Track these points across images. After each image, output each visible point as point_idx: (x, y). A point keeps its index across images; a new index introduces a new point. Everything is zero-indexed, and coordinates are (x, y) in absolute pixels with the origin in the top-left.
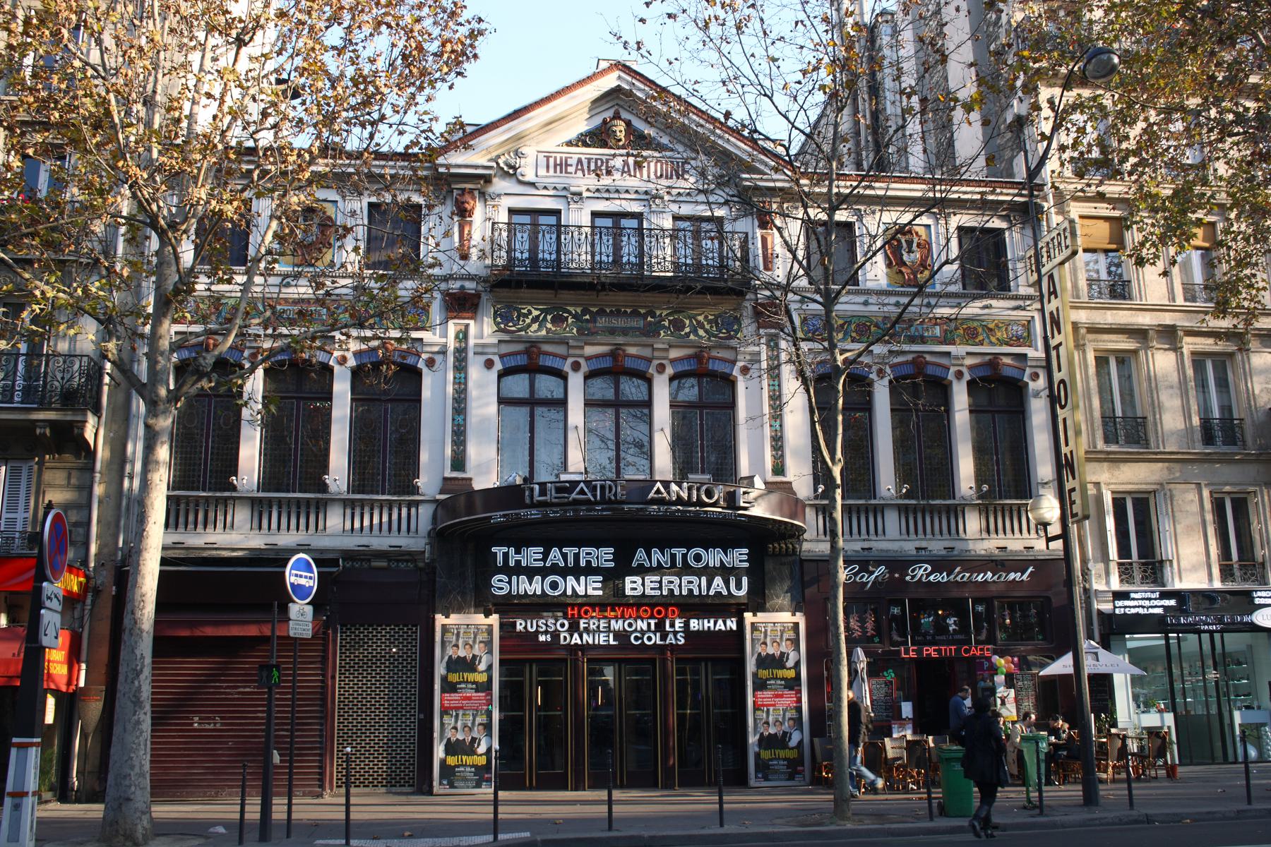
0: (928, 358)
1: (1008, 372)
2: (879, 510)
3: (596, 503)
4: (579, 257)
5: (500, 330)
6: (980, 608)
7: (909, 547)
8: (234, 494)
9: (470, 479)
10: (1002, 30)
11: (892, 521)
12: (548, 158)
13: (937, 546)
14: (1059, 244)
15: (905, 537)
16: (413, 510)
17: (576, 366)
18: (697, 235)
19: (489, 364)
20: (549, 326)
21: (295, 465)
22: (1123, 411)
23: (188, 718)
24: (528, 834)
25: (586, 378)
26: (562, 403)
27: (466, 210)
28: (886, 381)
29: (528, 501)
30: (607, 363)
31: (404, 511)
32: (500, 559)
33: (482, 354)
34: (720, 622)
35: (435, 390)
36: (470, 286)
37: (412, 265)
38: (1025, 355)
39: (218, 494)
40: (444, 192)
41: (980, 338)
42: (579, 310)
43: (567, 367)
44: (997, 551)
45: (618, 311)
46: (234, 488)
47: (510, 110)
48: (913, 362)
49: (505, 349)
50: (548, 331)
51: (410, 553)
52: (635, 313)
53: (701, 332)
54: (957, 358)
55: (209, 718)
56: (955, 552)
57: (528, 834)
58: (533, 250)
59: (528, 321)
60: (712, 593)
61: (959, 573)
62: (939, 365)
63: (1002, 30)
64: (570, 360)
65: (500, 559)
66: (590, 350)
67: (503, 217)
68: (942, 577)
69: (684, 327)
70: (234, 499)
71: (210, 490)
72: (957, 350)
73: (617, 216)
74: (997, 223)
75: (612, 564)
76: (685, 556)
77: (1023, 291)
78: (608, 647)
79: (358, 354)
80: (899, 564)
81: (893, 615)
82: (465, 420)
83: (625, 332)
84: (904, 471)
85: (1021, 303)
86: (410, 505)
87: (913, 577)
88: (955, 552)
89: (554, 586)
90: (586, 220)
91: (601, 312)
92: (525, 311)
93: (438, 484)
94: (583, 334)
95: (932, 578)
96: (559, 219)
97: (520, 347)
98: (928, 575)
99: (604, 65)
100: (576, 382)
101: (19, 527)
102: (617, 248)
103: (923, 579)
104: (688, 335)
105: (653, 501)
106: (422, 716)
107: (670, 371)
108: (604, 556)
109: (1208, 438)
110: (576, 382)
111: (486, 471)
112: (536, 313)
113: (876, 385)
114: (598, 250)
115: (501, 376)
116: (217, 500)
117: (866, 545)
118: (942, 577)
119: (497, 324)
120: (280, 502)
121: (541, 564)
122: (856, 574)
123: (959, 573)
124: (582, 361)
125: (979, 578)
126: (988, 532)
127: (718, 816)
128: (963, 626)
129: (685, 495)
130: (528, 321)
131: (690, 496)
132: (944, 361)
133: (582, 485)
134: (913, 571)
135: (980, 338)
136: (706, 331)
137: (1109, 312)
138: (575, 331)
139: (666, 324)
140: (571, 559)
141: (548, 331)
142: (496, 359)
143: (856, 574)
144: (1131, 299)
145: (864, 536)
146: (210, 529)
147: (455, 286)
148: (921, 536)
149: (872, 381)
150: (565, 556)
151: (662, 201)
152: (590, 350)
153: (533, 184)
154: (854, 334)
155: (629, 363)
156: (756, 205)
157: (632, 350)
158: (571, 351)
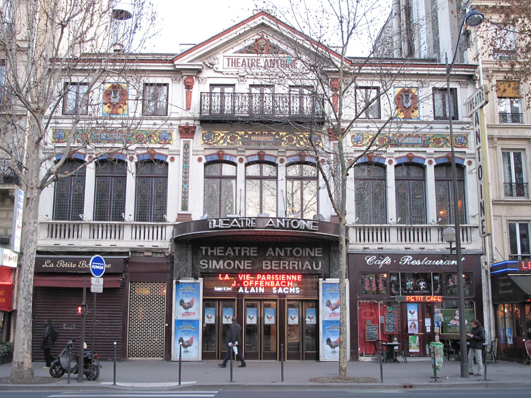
0: (415, 154)
3: (242, 228)
6: (437, 278)
7: (401, 247)
8: (82, 222)
9: (190, 215)
12: (229, 59)
13: (416, 247)
14: (480, 97)
16: (164, 229)
19: (200, 160)
20: (229, 141)
21: (109, 208)
22: (516, 181)
23: (61, 324)
24: (195, 382)
28: (133, 164)
29: (210, 227)
31: (160, 229)
33: (196, 155)
34: (264, 276)
35: (174, 171)
36: (191, 123)
37: (162, 113)
39: (74, 222)
40: (179, 77)
41: (442, 144)
42: (243, 133)
43: (278, 162)
44: (419, 250)
46: (81, 219)
47: (210, 37)
48: (407, 156)
49: (208, 152)
50: (228, 143)
51: (162, 249)
53: (302, 143)
55: (70, 325)
56: (425, 250)
57: (195, 382)
58: (301, 107)
59: (218, 139)
60: (304, 268)
61: (426, 261)
62: (420, 158)
64: (238, 157)
66: (248, 153)
68: (418, 263)
69: (293, 141)
70: (82, 224)
72: (391, 150)
77: (466, 120)
78: (295, 294)
80: (396, 256)
81: (393, 281)
82: (188, 186)
85: (464, 126)
87: (403, 262)
88: (425, 250)
89: (229, 265)
92: (217, 134)
93: (176, 217)
94: (245, 145)
95: (412, 263)
96: (234, 89)
97: (215, 151)
98: (411, 261)
103: (408, 263)
104: (295, 144)
105: (268, 227)
106: (167, 325)
108: (252, 252)
111: (197, 213)
112: (222, 135)
114: (292, 105)
115: (206, 165)
117: (380, 246)
118: (418, 263)
119: (204, 140)
121: (223, 254)
123: (426, 261)
125: (436, 263)
127: (116, 380)
128: (428, 288)
129: (283, 225)
130: (218, 139)
132: (423, 155)
133: (235, 220)
134: (403, 259)
135: (442, 144)
136: (304, 143)
137: (510, 130)
138: (241, 143)
139: (285, 139)
141: (228, 143)
143: (374, 261)
146: (71, 238)
147: (183, 123)
149: (465, 166)
152: (248, 153)
154: (229, 141)
158: (280, 154)
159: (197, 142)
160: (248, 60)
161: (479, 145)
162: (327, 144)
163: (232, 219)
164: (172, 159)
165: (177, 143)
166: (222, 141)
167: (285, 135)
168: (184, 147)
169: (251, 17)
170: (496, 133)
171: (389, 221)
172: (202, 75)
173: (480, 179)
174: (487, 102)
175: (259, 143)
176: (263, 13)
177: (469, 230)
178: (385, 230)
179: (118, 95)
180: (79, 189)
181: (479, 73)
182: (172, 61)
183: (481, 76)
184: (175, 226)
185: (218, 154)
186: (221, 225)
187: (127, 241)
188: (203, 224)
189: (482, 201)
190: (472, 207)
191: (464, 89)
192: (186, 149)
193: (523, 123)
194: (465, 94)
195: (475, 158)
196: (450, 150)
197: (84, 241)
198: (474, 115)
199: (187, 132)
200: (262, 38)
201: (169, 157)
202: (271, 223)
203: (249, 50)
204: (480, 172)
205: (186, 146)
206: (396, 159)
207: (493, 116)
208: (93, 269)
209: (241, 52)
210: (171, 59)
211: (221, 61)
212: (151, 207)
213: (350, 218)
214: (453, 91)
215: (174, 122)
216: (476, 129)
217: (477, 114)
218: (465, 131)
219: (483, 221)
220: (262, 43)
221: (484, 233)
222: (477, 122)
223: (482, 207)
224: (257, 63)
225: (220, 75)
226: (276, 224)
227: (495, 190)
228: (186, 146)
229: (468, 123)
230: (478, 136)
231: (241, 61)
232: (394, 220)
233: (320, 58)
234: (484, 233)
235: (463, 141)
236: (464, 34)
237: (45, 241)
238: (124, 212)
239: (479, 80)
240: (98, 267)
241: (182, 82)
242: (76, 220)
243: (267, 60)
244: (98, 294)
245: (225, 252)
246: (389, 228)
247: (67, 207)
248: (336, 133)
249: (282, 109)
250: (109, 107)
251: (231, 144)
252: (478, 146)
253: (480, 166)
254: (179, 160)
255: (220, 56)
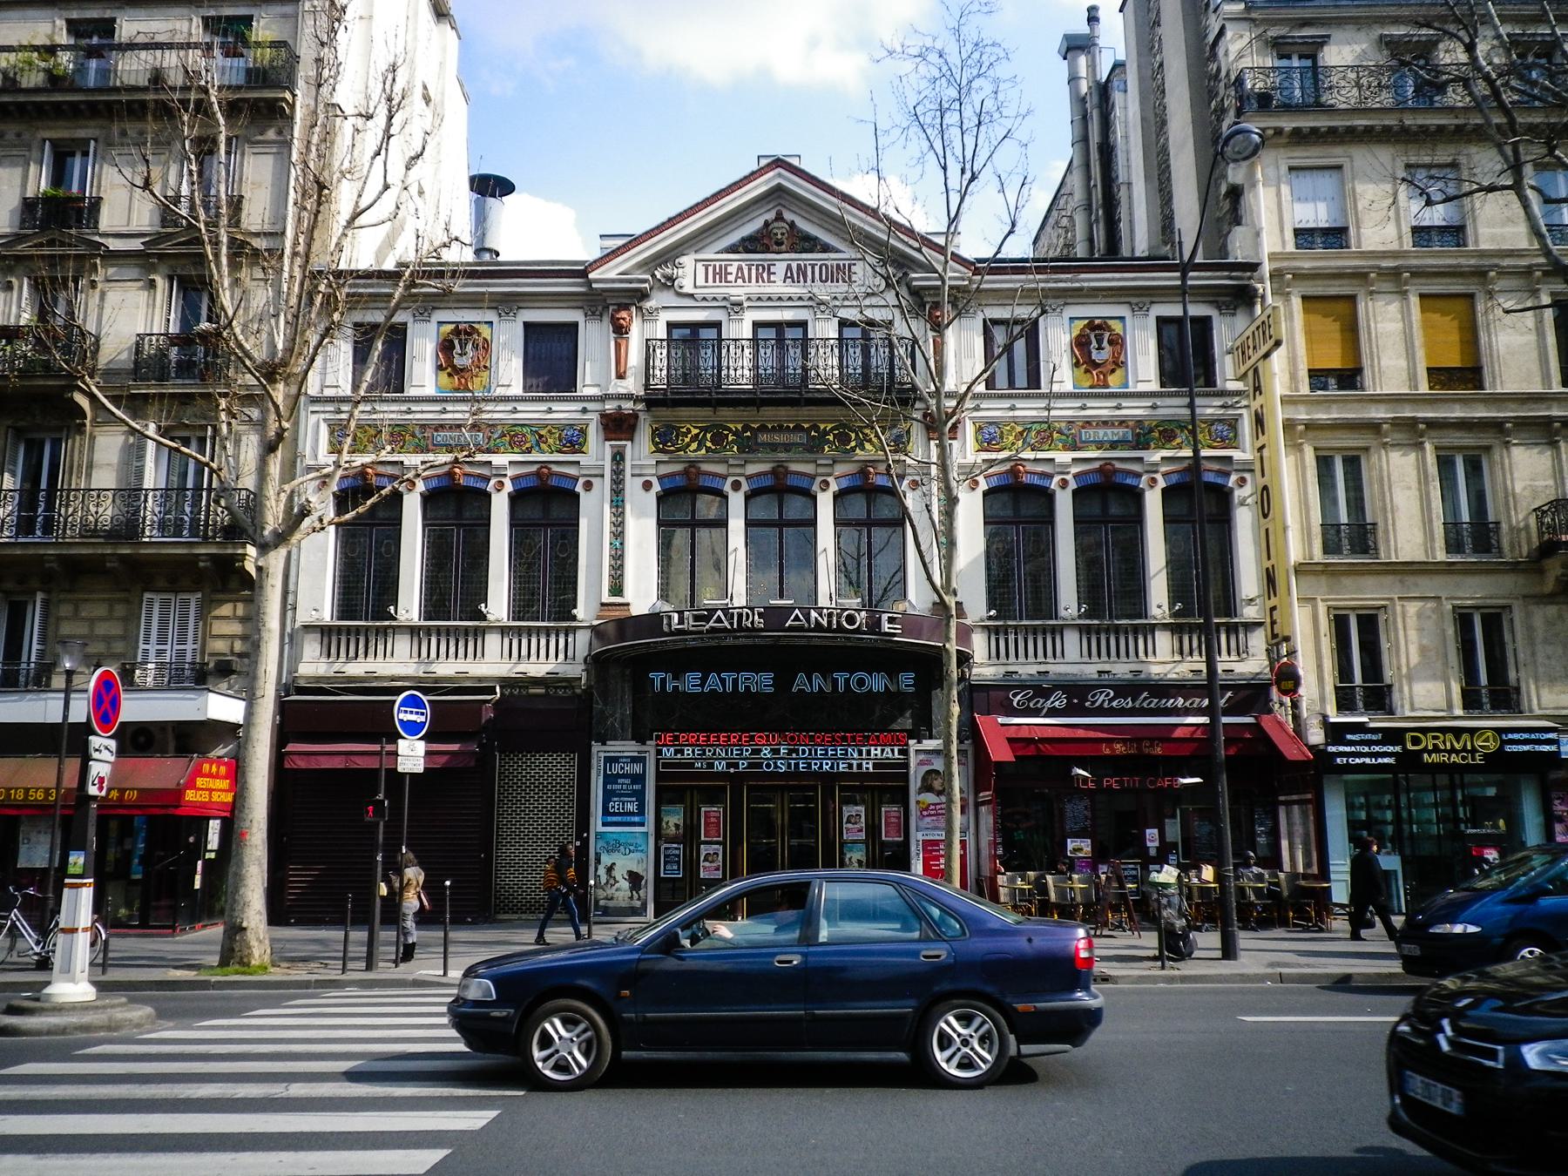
0: (1118, 465)
1: (1209, 477)
2: (1152, 628)
3: (734, 631)
4: (740, 371)
5: (658, 451)
7: (1090, 671)
10: (1222, 84)
11: (1072, 640)
13: (1121, 670)
15: (1086, 659)
17: (736, 486)
18: (780, 341)
19: (647, 486)
20: (709, 444)
21: (456, 591)
25: (748, 498)
26: (722, 523)
27: (622, 326)
28: (978, 496)
29: (666, 628)
30: (768, 482)
31: (1012, 637)
32: (657, 684)
36: (628, 406)
38: (1230, 458)
41: (1178, 440)
42: (739, 427)
44: (1190, 676)
45: (781, 427)
49: (664, 470)
50: (708, 450)
52: (798, 428)
54: (1062, 465)
63: (1222, 84)
64: (730, 480)
65: (657, 684)
66: (752, 469)
67: (662, 333)
71: (373, 619)
73: (778, 326)
74: (1196, 310)
75: (772, 690)
76: (847, 681)
77: (1233, 386)
79: (514, 479)
83: (787, 447)
84: (1178, 591)
86: (567, 631)
88: (1143, 676)
90: (747, 332)
91: (763, 428)
95: (1114, 704)
96: (805, 332)
97: (678, 468)
98: (1111, 701)
99: (764, 162)
100: (736, 501)
101: (189, 659)
102: (781, 358)
103: (1106, 705)
104: (853, 449)
105: (791, 628)
107: (834, 487)
109: (1453, 545)
110: (736, 501)
111: (642, 596)
112: (695, 431)
113: (493, 497)
116: (378, 630)
117: (1042, 668)
119: (656, 444)
120: (438, 630)
122: (1029, 700)
124: (742, 480)
126: (1181, 653)
129: (825, 623)
131: (830, 622)
132: (572, 471)
133: (719, 613)
139: (1156, 435)
140: (729, 688)
141: (708, 450)
142: (654, 480)
144: (1362, 389)
145: (1041, 658)
147: (610, 406)
148: (1104, 657)
150: (723, 681)
151: (824, 307)
153: (691, 296)
154: (709, 444)
155: (791, 481)
156: (929, 306)
157: (794, 467)
158: (732, 470)
159: (641, 451)
160: (813, 267)
161: (1262, 440)
162: (921, 449)
163: (712, 611)
164: (588, 486)
165: (597, 452)
166: (694, 446)
167: (832, 429)
168: (614, 458)
169: (753, 173)
170: (1302, 415)
171: (1062, 613)
172: (649, 304)
173: (1265, 516)
174: (1278, 344)
175: (774, 447)
176: (778, 163)
177: (1241, 629)
178: (1053, 633)
179: (1105, 344)
180: (388, 552)
181: (1262, 281)
182: (583, 274)
183: (1265, 287)
184: (593, 628)
185: (686, 472)
186: (689, 624)
187: (493, 662)
188: (652, 621)
189: (1268, 564)
190: (1248, 582)
191: (1228, 319)
192: (618, 464)
193: (1362, 389)
194: (1226, 332)
195: (1252, 471)
196: (1188, 453)
197: (396, 661)
198: (1251, 373)
199: (618, 426)
200: (779, 217)
201: (581, 481)
202: (797, 619)
203: (751, 244)
204: (1266, 502)
205: (618, 458)
206: (748, 478)
207: (1293, 377)
208: (401, 721)
209: (732, 249)
210: (581, 272)
211: (690, 272)
212: (547, 587)
213: (976, 604)
214: (1204, 324)
215: (590, 406)
216: (1255, 405)
217: (1256, 371)
218: (1231, 412)
219: (1273, 609)
220: (780, 230)
221: (1274, 636)
222: (1257, 389)
223: (1270, 580)
224: (770, 273)
225: (691, 303)
226: (808, 620)
227: (1299, 544)
228: (618, 458)
229: (1238, 393)
230: (1259, 421)
231: (733, 269)
232: (1073, 611)
233: (898, 256)
234: (1274, 636)
235: (1228, 431)
236: (1228, 194)
237: (314, 664)
238: (486, 601)
239: (1263, 297)
240: (413, 717)
241: (606, 319)
242: (564, 620)
243: (789, 267)
244: (412, 775)
245: (702, 685)
246: (1062, 627)
247: (366, 588)
248: (939, 426)
249: (822, 372)
250: (450, 375)
251: (714, 451)
252: (1259, 444)
253: (1265, 488)
254: (604, 487)
255: (687, 260)
